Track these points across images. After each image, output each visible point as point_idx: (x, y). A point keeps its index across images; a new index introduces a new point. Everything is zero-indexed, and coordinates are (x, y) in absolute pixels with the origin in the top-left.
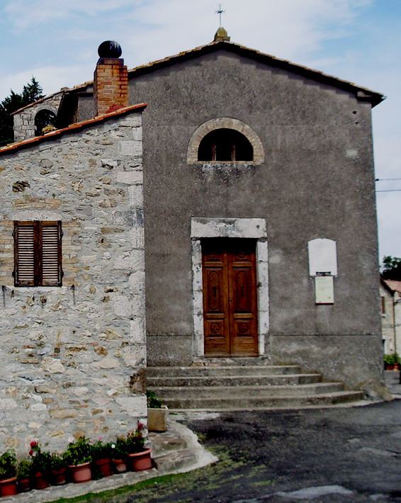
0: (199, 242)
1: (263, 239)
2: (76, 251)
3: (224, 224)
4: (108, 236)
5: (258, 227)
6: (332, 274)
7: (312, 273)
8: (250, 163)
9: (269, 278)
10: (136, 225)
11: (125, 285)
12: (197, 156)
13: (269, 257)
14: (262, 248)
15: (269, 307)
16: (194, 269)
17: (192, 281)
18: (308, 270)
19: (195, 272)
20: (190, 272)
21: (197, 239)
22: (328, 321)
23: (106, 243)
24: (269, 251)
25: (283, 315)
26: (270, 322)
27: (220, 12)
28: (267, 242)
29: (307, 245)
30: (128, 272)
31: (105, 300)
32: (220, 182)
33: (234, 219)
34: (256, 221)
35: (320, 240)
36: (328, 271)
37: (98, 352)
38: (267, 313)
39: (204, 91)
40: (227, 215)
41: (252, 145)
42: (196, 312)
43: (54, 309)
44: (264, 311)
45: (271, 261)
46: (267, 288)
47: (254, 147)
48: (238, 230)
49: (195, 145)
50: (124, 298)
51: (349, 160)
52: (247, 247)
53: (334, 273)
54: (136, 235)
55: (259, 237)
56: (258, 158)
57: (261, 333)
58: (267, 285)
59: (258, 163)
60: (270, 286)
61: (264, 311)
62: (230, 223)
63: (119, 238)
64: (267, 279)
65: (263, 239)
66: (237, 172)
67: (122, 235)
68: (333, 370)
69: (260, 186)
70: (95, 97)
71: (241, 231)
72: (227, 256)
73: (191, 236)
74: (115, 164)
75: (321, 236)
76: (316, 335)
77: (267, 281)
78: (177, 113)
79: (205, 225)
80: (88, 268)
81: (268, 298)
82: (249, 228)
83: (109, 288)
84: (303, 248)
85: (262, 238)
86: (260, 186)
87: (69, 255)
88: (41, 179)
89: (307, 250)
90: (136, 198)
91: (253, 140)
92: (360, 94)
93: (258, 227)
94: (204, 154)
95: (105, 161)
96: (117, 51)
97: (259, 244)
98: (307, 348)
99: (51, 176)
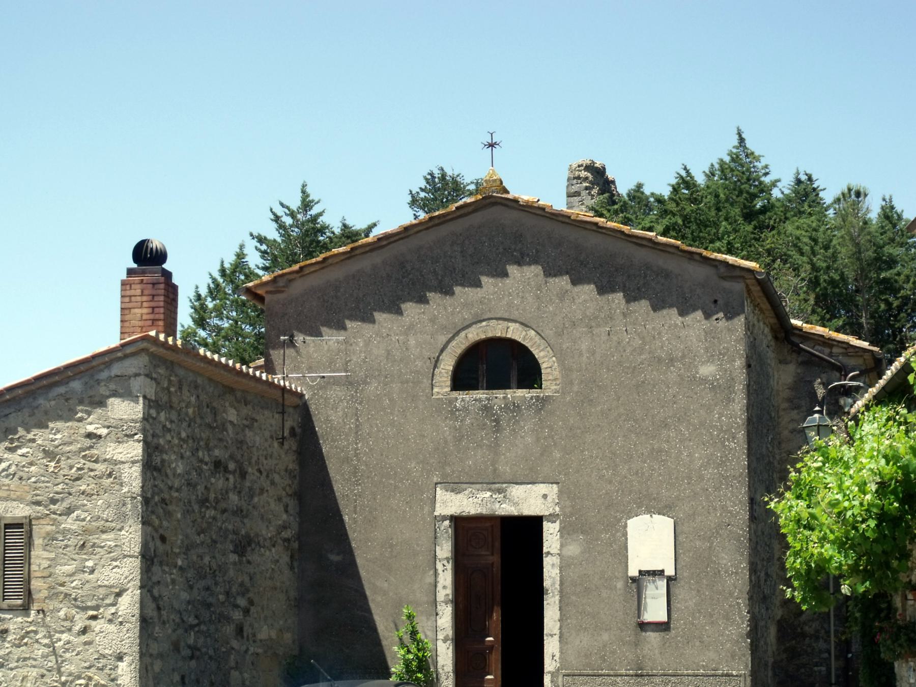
0: (447, 523)
1: (552, 518)
2: (48, 559)
4: (93, 539)
5: (545, 496)
6: (667, 573)
8: (534, 392)
10: (131, 522)
11: (113, 610)
12: (449, 383)
13: (562, 546)
15: (560, 628)
16: (439, 566)
17: (436, 586)
18: (627, 566)
20: (432, 572)
21: (444, 518)
23: (88, 548)
24: (561, 537)
25: (582, 641)
26: (561, 652)
27: (492, 145)
28: (558, 522)
29: (626, 526)
30: (117, 590)
31: (84, 631)
32: (485, 424)
34: (542, 488)
36: (660, 569)
38: (557, 638)
39: (463, 276)
40: (496, 483)
41: (540, 361)
42: (441, 636)
43: (17, 642)
44: (552, 636)
45: (564, 552)
46: (557, 598)
47: (543, 366)
48: (516, 504)
49: (447, 365)
50: (112, 628)
51: (704, 380)
52: (524, 534)
54: (131, 536)
55: (547, 513)
56: (548, 383)
59: (548, 393)
61: (552, 636)
62: (500, 491)
63: (108, 539)
65: (552, 518)
66: (514, 408)
67: (111, 536)
69: (551, 428)
71: (516, 504)
72: (896, 508)
73: (436, 514)
74: (103, 432)
75: (650, 511)
76: (637, 675)
78: (420, 314)
79: (460, 496)
80: (62, 585)
81: (559, 613)
82: (528, 500)
83: (91, 613)
84: (617, 531)
86: (551, 428)
87: (39, 566)
88: (6, 456)
89: (625, 535)
90: (133, 478)
91: (542, 354)
94: (463, 379)
95: (91, 428)
96: (160, 257)
97: (546, 525)
99: (20, 452)
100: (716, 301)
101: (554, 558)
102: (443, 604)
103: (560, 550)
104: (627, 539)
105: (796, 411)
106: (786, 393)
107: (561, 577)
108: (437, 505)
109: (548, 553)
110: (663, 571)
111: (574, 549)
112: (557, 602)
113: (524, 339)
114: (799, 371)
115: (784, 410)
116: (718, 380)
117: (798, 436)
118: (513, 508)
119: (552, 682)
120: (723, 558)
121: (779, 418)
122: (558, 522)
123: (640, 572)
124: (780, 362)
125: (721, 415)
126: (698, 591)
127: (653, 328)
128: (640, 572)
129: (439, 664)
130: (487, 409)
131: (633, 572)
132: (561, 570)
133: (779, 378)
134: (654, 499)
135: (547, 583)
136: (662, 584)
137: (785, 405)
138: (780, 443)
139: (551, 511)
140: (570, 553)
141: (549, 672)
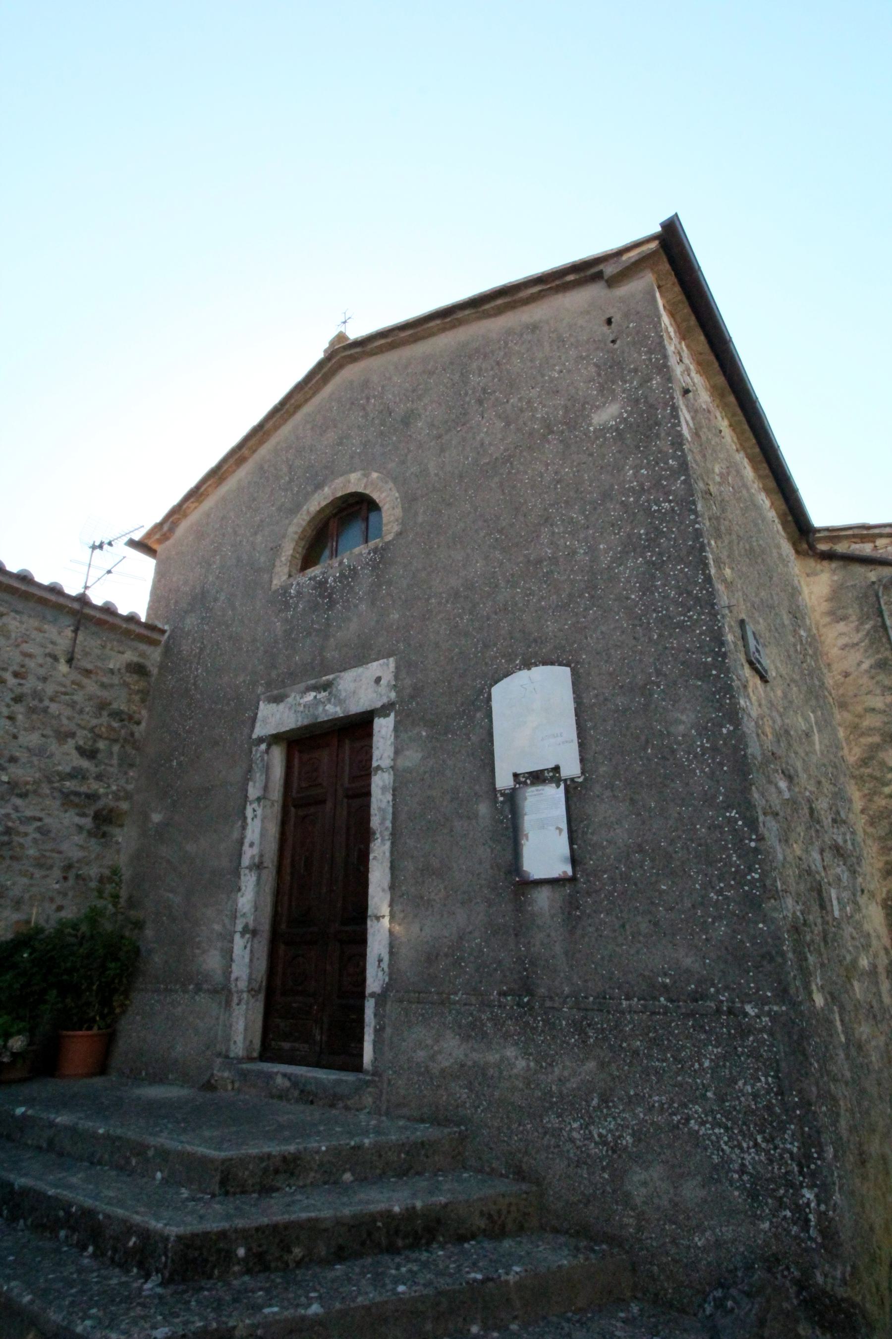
1: (384, 711)
3: (313, 694)
5: (378, 680)
6: (565, 773)
7: (504, 781)
9: (394, 813)
13: (397, 752)
14: (384, 727)
19: (249, 820)
22: (558, 949)
28: (392, 715)
29: (489, 699)
33: (331, 677)
34: (375, 668)
35: (524, 673)
37: (608, 1092)
46: (388, 844)
48: (340, 702)
53: (571, 768)
55: (378, 705)
57: (368, 991)
58: (387, 834)
60: (395, 836)
62: (327, 686)
64: (390, 817)
65: (384, 711)
68: (106, 1102)
70: (842, 699)
77: (388, 824)
85: (383, 706)
92: (609, 270)
93: (378, 680)
98: (492, 1057)
100: (609, 322)
101: (386, 775)
102: (247, 871)
103: (394, 760)
104: (491, 721)
105: (842, 624)
106: (825, 606)
107: (394, 806)
108: (258, 725)
109: (378, 768)
110: (557, 769)
111: (412, 757)
112: (388, 854)
113: (365, 487)
114: (836, 578)
115: (825, 626)
116: (625, 419)
117: (852, 651)
118: (338, 709)
119: (375, 1015)
120: (679, 722)
121: (820, 636)
122: (392, 715)
123: (516, 776)
124: (808, 575)
125: (637, 468)
126: (633, 801)
127: (520, 399)
128: (516, 776)
129: (233, 976)
130: (321, 585)
131: (504, 781)
132: (394, 795)
133: (811, 593)
134: (535, 641)
135: (375, 822)
136: (555, 794)
137: (827, 619)
138: (829, 665)
139: (385, 700)
140: (408, 764)
141: (373, 995)
